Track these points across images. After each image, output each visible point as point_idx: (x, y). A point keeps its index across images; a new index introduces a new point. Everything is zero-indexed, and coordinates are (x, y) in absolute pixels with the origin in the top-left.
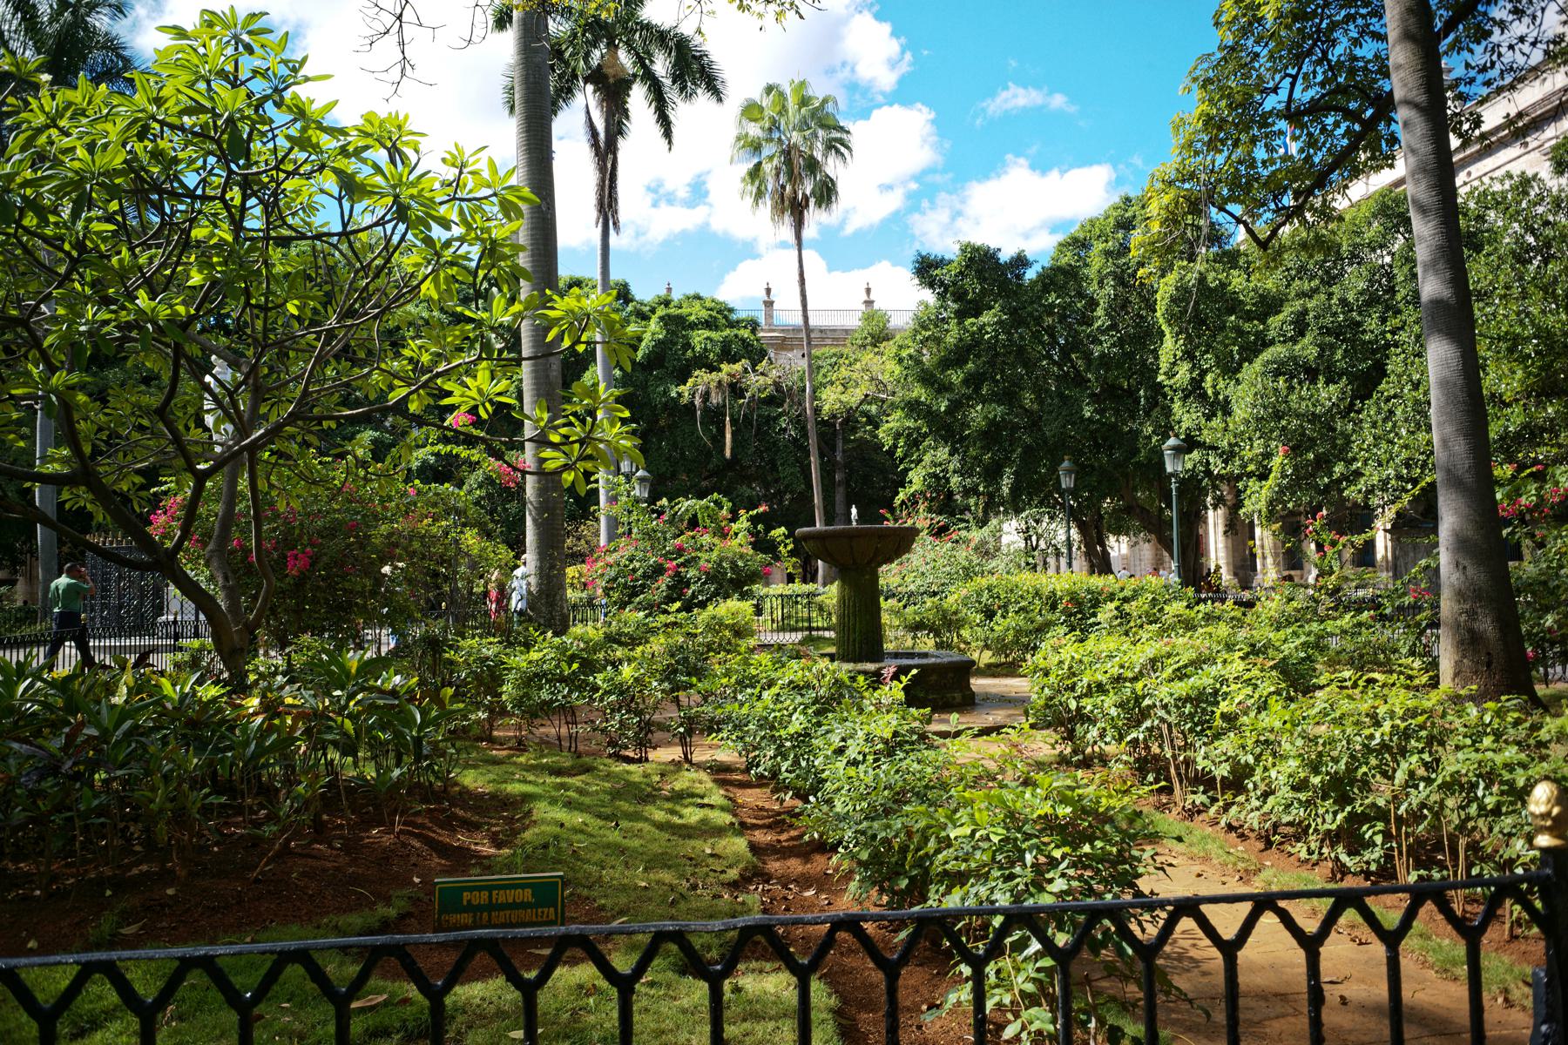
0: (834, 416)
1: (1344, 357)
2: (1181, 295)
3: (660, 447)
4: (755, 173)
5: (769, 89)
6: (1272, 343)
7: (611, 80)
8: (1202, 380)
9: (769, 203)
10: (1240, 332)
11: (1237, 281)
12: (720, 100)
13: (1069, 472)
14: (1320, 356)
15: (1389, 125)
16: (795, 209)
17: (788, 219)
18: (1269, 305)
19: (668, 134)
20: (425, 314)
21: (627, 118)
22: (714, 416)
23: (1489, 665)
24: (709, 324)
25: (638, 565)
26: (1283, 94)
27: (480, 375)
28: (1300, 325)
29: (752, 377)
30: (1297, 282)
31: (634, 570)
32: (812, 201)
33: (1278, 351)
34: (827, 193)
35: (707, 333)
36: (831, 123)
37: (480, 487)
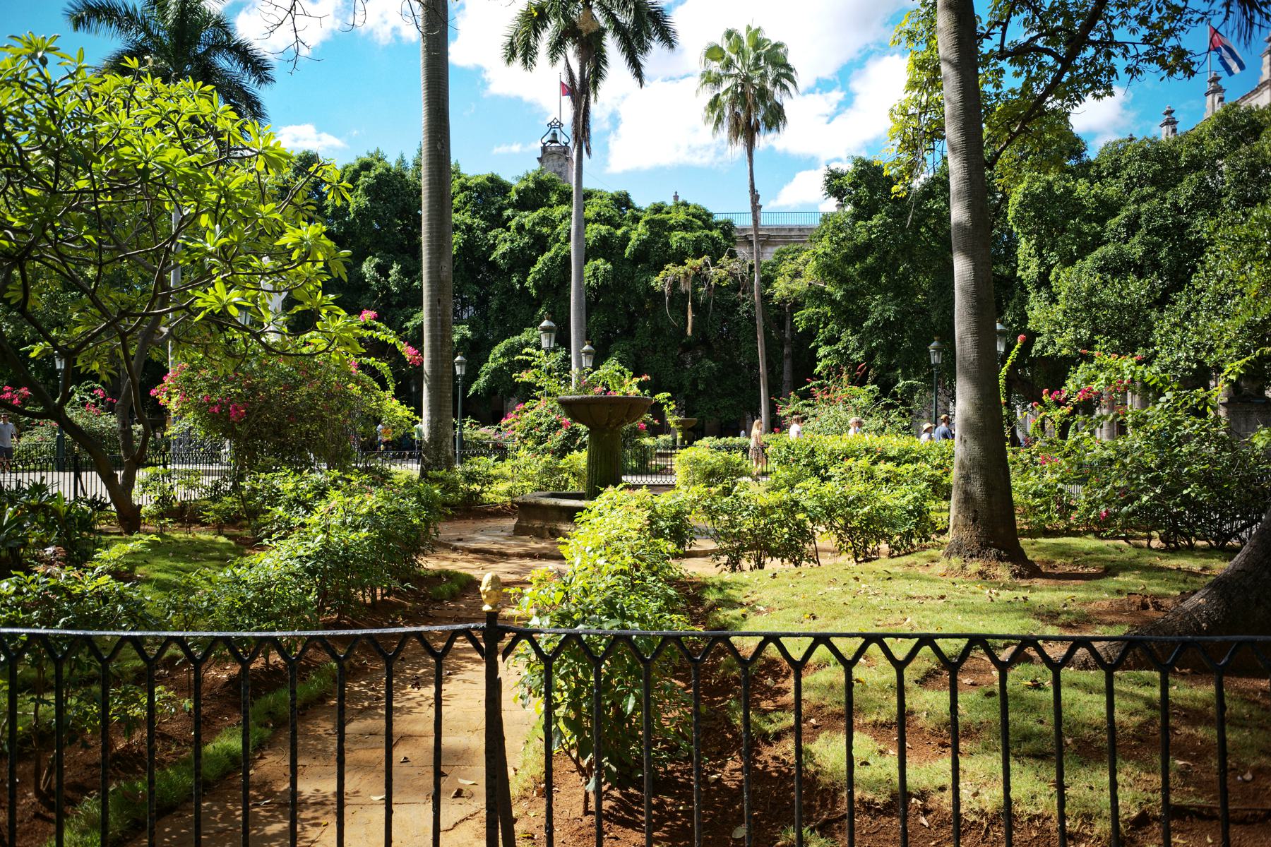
0: (784, 301)
1: (1168, 254)
2: (1031, 201)
3: (645, 326)
4: (714, 104)
5: (729, 34)
6: (1105, 243)
7: (584, 35)
8: (1049, 273)
9: (726, 129)
10: (1079, 233)
11: (1081, 187)
12: (672, 47)
13: (937, 350)
14: (1146, 253)
15: (1109, 59)
16: (746, 131)
17: (741, 140)
18: (1108, 208)
19: (639, 74)
20: (468, 221)
21: (605, 63)
22: (678, 299)
23: (974, 520)
24: (686, 227)
25: (542, 419)
26: (997, 39)
27: (217, 286)
28: (1132, 226)
29: (712, 270)
30: (1137, 189)
31: (540, 424)
32: (762, 127)
33: (1110, 249)
34: (776, 117)
35: (682, 234)
36: (781, 61)
37: (503, 355)
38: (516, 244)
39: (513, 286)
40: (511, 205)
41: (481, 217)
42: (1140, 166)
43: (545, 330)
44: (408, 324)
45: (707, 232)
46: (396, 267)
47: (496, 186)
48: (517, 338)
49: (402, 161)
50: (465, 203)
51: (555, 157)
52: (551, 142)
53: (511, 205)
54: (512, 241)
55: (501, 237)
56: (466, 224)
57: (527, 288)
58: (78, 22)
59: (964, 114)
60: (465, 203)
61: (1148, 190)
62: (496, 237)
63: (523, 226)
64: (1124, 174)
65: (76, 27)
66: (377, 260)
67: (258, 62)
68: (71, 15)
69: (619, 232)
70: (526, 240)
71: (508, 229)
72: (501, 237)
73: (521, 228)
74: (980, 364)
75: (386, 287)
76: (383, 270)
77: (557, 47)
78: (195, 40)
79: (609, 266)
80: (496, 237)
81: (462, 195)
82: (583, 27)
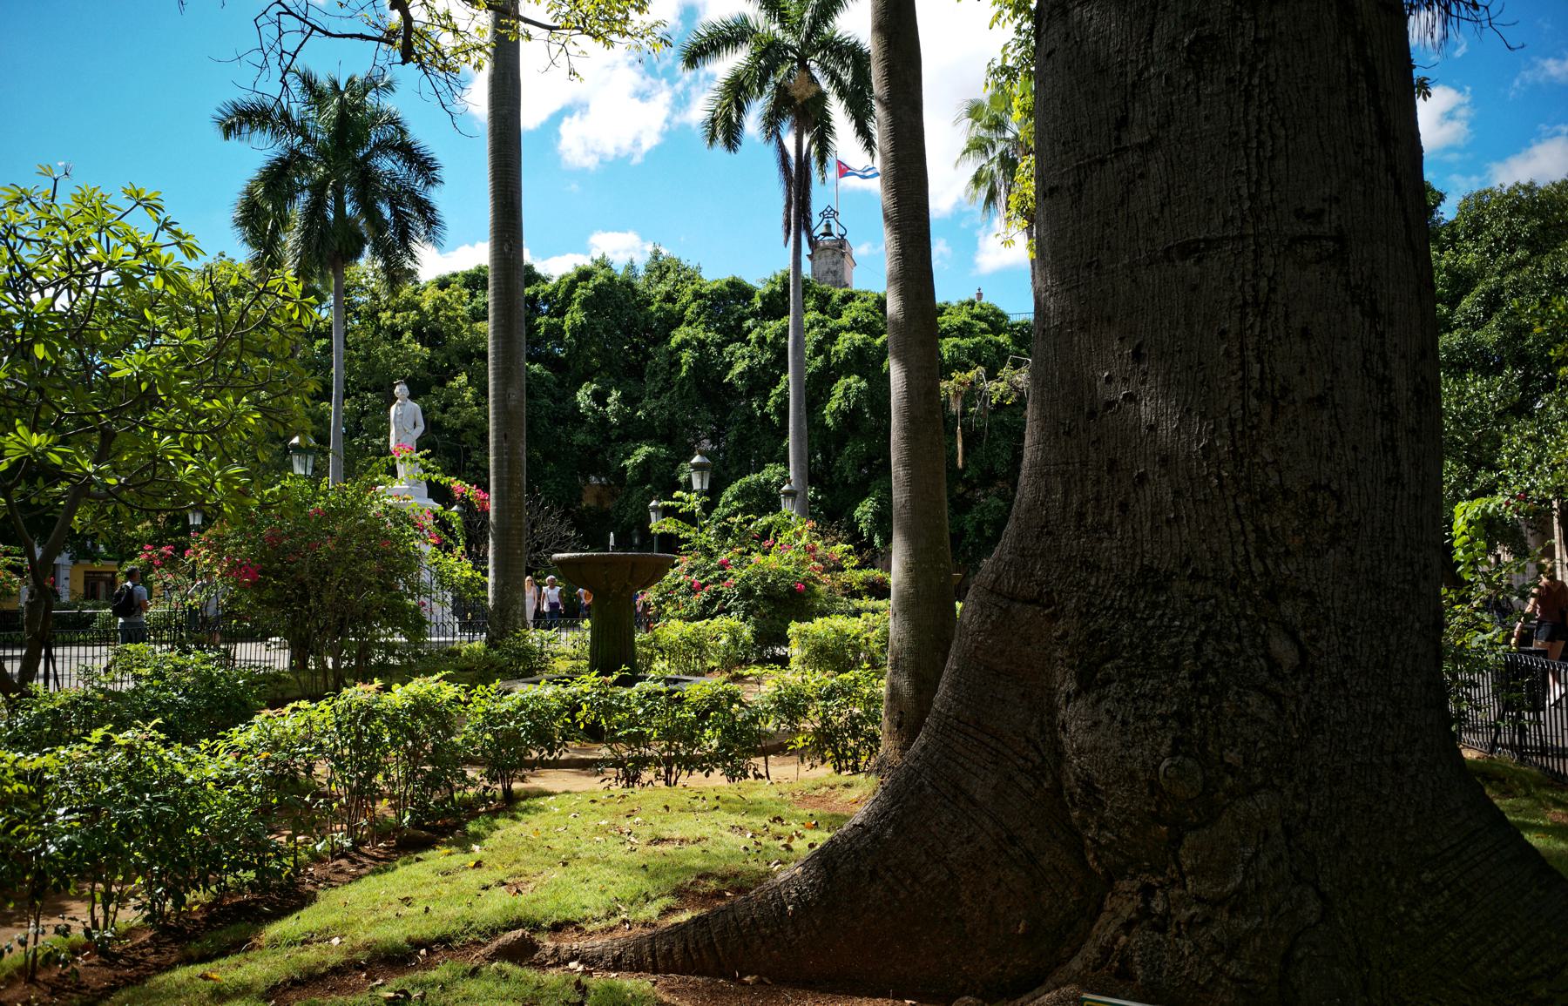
7: (799, 102)
20: (701, 336)
31: (679, 585)
35: (956, 340)
37: (736, 498)
38: (756, 361)
39: (753, 412)
40: (754, 314)
41: (718, 331)
42: (1509, 224)
43: (697, 467)
44: (627, 462)
45: (991, 337)
46: (615, 394)
47: (739, 291)
48: (754, 477)
49: (631, 267)
50: (699, 314)
51: (829, 253)
52: (825, 234)
53: (754, 314)
54: (752, 358)
55: (738, 353)
56: (698, 340)
57: (767, 415)
58: (228, 130)
59: (895, 167)
60: (699, 314)
61: (1520, 254)
62: (732, 354)
63: (764, 338)
64: (1485, 236)
65: (227, 136)
66: (594, 386)
67: (425, 162)
68: (221, 122)
69: (878, 342)
70: (768, 355)
71: (748, 343)
72: (738, 353)
73: (762, 341)
74: (913, 508)
75: (604, 420)
76: (600, 397)
77: (772, 123)
78: (361, 141)
79: (863, 384)
80: (732, 354)
81: (694, 305)
82: (796, 93)
